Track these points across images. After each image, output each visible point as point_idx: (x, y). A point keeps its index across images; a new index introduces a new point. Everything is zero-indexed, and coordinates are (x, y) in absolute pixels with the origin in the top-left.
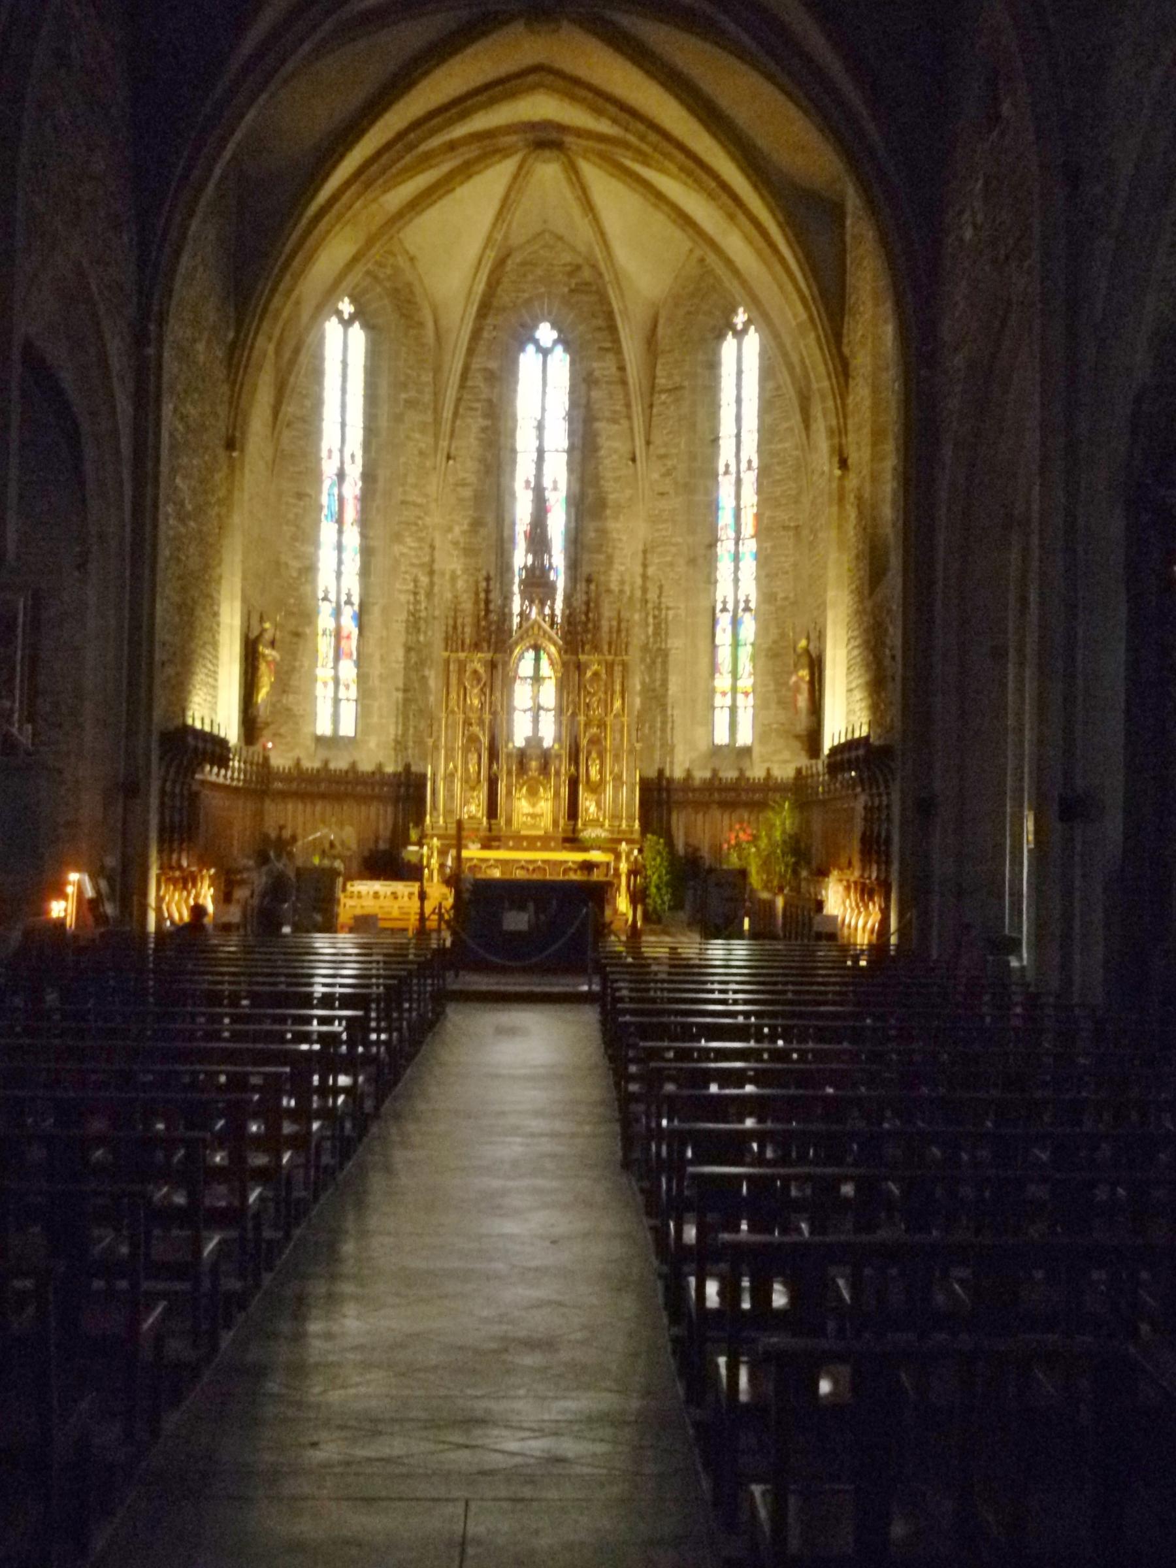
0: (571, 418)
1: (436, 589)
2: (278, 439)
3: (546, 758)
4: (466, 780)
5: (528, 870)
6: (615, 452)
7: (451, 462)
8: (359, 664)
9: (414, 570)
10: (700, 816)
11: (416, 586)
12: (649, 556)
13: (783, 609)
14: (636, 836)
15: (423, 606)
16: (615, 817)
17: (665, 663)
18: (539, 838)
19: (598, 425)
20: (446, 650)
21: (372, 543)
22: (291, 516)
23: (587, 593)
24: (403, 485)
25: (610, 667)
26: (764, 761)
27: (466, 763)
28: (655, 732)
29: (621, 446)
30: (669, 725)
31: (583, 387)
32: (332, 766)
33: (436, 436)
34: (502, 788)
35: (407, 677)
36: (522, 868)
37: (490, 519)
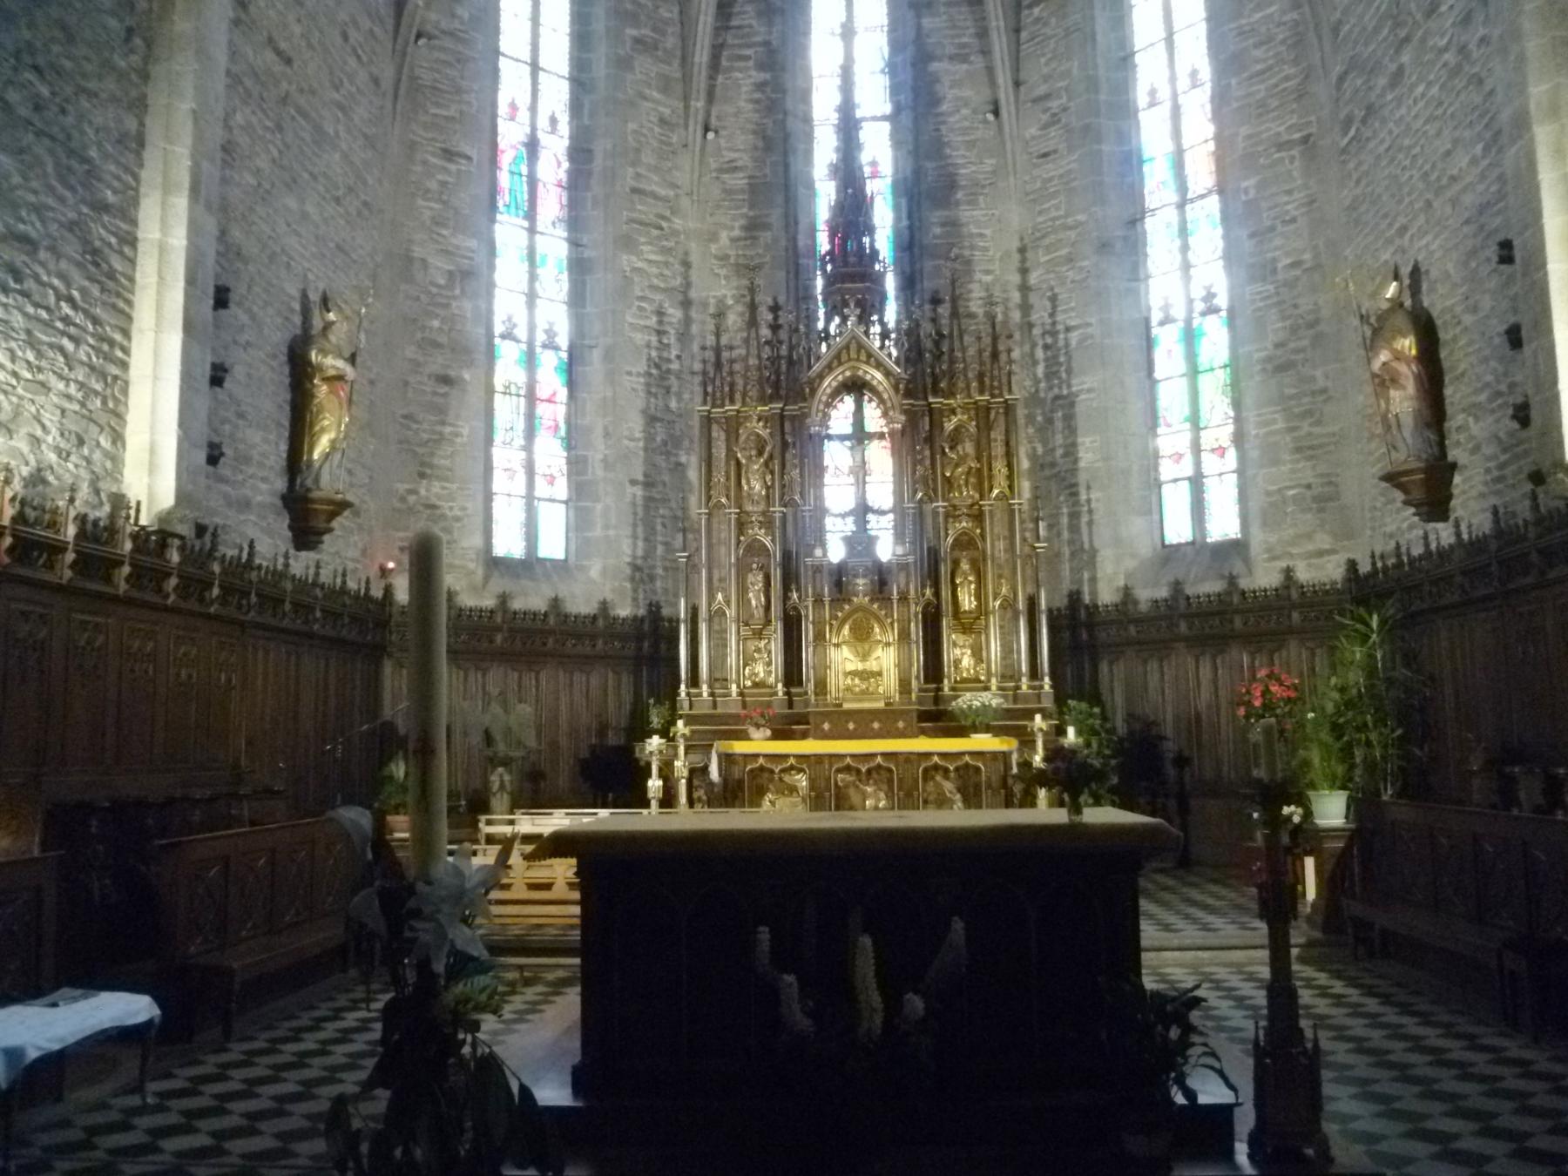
0: (892, 68)
1: (695, 329)
2: (404, 54)
3: (881, 578)
4: (744, 621)
5: (858, 771)
6: (966, 105)
7: (711, 135)
8: (570, 443)
9: (658, 297)
10: (1153, 665)
11: (660, 322)
12: (1029, 255)
13: (1290, 284)
14: (1048, 703)
15: (674, 353)
16: (1010, 674)
17: (1069, 418)
18: (874, 714)
19: (935, 66)
20: (705, 403)
21: (587, 253)
22: (433, 185)
23: (934, 320)
24: (633, 164)
25: (985, 425)
26: (1274, 558)
27: (743, 590)
28: (1059, 535)
29: (975, 95)
30: (1085, 519)
31: (910, 15)
32: (517, 605)
33: (686, 98)
34: (808, 632)
35: (650, 464)
36: (848, 769)
37: (775, 216)
